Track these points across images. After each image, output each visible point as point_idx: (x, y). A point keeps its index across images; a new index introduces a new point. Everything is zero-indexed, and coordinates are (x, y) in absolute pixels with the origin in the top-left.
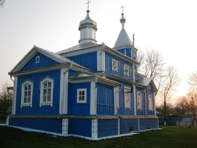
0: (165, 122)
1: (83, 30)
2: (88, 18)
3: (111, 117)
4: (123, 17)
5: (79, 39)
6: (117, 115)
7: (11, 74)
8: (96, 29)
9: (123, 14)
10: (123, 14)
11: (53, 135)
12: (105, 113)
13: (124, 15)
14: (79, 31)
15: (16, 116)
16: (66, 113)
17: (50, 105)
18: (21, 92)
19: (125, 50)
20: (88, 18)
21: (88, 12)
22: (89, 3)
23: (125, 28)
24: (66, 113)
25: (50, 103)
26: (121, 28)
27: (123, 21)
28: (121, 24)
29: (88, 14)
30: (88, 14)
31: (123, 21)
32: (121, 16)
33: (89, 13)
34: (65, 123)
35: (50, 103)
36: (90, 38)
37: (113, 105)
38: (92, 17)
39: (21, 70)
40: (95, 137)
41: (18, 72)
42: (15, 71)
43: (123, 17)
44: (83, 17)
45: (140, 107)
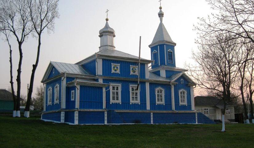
0: (25, 108)
1: (102, 37)
2: (107, 26)
3: (100, 110)
4: (161, 11)
5: (100, 46)
6: (105, 109)
7: (42, 82)
8: (114, 36)
9: (161, 8)
10: (161, 8)
11: (53, 122)
12: (84, 108)
13: (162, 9)
14: (99, 38)
15: (46, 112)
16: (65, 108)
17: (119, 103)
18: (129, 91)
19: (158, 46)
20: (107, 26)
21: (107, 20)
22: (108, 12)
23: (163, 22)
24: (65, 108)
25: (138, 102)
26: (160, 22)
27: (161, 15)
28: (159, 18)
29: (107, 22)
30: (107, 22)
31: (161, 15)
32: (159, 10)
33: (108, 21)
34: (63, 114)
35: (138, 102)
36: (106, 45)
37: (145, 103)
38: (111, 25)
39: (48, 79)
40: (76, 122)
41: (45, 81)
42: (44, 80)
43: (161, 11)
44: (102, 26)
45: (49, 103)
